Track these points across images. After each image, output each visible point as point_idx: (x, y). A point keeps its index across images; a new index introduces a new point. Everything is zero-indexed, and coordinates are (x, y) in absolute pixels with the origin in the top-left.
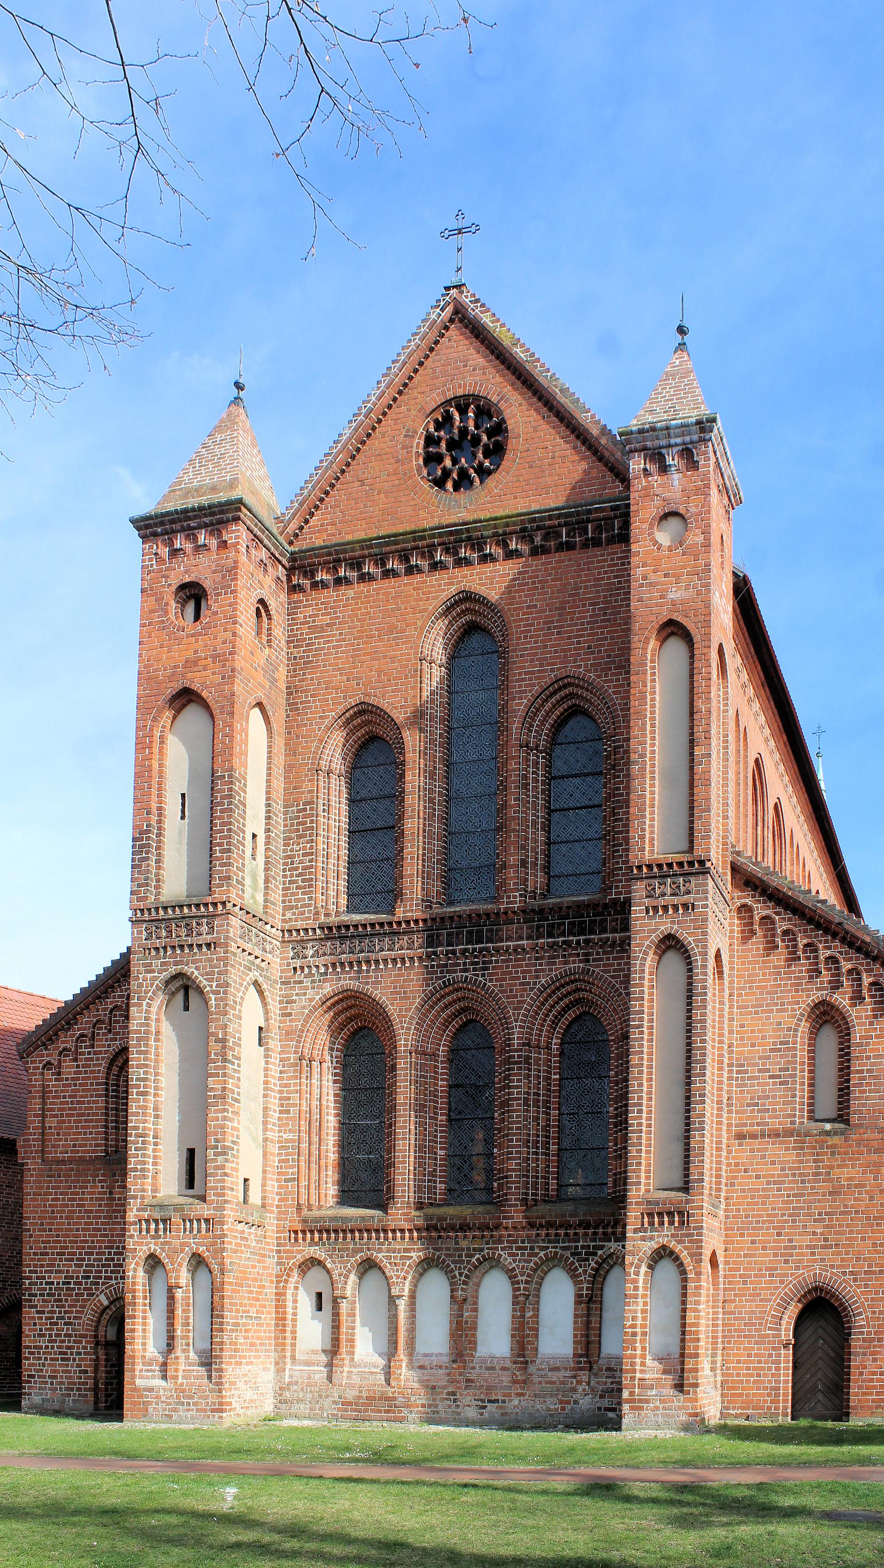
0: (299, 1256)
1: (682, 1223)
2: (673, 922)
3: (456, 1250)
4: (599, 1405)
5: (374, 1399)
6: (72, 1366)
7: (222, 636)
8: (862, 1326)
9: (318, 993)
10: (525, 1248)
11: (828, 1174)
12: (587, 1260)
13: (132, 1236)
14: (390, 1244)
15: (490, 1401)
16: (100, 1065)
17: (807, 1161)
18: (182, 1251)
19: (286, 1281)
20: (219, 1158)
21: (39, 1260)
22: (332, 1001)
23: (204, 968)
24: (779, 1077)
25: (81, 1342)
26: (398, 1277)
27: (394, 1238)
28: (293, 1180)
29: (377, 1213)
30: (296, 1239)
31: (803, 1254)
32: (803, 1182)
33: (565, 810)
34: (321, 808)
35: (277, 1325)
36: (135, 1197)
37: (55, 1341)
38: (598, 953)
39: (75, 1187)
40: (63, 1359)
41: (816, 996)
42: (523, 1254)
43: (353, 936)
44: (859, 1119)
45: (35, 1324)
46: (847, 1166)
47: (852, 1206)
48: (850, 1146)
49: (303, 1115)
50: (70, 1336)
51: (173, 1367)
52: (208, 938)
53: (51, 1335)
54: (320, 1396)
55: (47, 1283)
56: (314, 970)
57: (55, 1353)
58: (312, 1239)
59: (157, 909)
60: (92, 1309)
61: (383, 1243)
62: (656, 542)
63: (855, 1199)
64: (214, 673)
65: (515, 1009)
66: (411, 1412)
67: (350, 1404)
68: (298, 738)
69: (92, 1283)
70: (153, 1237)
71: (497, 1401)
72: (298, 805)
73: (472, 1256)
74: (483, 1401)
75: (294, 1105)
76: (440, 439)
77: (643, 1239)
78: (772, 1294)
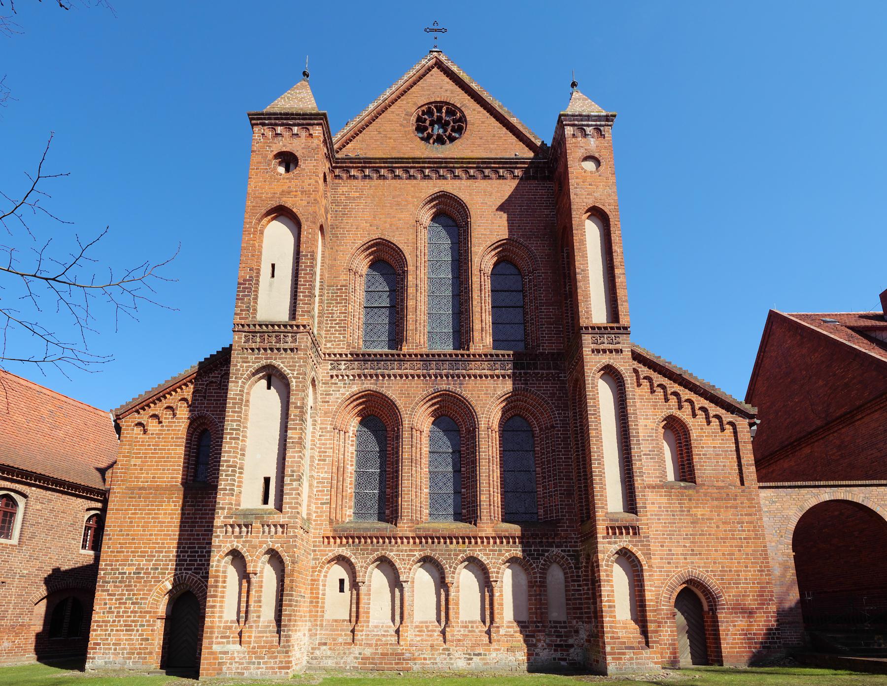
0: (330, 554)
1: (635, 534)
2: (610, 358)
3: (446, 550)
4: (554, 656)
5: (387, 654)
6: (135, 635)
7: (307, 181)
8: (723, 605)
9: (348, 391)
10: (495, 551)
11: (689, 511)
12: (539, 559)
13: (218, 536)
14: (399, 546)
15: (475, 655)
16: (181, 426)
17: (674, 503)
18: (260, 547)
19: (320, 571)
20: (294, 483)
21: (115, 556)
22: (357, 396)
23: (288, 362)
24: (649, 455)
25: (145, 617)
26: (405, 568)
27: (402, 543)
28: (327, 503)
29: (389, 525)
30: (329, 543)
31: (679, 559)
32: (673, 515)
33: (500, 307)
34: (351, 290)
35: (311, 602)
36: (223, 509)
37: (122, 617)
38: (533, 380)
39: (152, 505)
40: (127, 630)
41: (666, 413)
42: (494, 554)
43: (373, 361)
44: (702, 481)
45: (105, 604)
46: (700, 507)
47: (706, 531)
48: (699, 496)
49: (334, 463)
50: (136, 612)
51: (247, 634)
52: (293, 345)
53: (118, 612)
54: (345, 653)
55: (120, 573)
56: (346, 378)
57: (121, 626)
58: (341, 543)
59: (254, 325)
60: (158, 593)
61: (393, 546)
62: (583, 169)
63: (708, 527)
64: (301, 200)
65: (481, 407)
66: (415, 664)
67: (367, 658)
68: (337, 251)
69: (159, 573)
70: (236, 537)
71: (479, 654)
72: (337, 286)
73: (458, 555)
74: (470, 654)
75: (330, 456)
76: (425, 119)
77: (609, 543)
78: (662, 583)
